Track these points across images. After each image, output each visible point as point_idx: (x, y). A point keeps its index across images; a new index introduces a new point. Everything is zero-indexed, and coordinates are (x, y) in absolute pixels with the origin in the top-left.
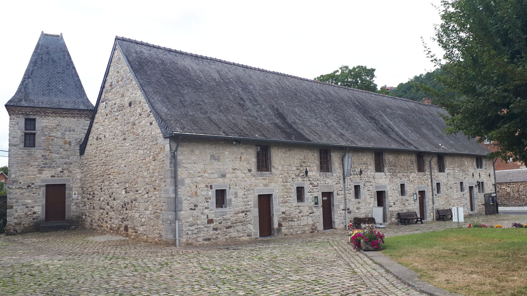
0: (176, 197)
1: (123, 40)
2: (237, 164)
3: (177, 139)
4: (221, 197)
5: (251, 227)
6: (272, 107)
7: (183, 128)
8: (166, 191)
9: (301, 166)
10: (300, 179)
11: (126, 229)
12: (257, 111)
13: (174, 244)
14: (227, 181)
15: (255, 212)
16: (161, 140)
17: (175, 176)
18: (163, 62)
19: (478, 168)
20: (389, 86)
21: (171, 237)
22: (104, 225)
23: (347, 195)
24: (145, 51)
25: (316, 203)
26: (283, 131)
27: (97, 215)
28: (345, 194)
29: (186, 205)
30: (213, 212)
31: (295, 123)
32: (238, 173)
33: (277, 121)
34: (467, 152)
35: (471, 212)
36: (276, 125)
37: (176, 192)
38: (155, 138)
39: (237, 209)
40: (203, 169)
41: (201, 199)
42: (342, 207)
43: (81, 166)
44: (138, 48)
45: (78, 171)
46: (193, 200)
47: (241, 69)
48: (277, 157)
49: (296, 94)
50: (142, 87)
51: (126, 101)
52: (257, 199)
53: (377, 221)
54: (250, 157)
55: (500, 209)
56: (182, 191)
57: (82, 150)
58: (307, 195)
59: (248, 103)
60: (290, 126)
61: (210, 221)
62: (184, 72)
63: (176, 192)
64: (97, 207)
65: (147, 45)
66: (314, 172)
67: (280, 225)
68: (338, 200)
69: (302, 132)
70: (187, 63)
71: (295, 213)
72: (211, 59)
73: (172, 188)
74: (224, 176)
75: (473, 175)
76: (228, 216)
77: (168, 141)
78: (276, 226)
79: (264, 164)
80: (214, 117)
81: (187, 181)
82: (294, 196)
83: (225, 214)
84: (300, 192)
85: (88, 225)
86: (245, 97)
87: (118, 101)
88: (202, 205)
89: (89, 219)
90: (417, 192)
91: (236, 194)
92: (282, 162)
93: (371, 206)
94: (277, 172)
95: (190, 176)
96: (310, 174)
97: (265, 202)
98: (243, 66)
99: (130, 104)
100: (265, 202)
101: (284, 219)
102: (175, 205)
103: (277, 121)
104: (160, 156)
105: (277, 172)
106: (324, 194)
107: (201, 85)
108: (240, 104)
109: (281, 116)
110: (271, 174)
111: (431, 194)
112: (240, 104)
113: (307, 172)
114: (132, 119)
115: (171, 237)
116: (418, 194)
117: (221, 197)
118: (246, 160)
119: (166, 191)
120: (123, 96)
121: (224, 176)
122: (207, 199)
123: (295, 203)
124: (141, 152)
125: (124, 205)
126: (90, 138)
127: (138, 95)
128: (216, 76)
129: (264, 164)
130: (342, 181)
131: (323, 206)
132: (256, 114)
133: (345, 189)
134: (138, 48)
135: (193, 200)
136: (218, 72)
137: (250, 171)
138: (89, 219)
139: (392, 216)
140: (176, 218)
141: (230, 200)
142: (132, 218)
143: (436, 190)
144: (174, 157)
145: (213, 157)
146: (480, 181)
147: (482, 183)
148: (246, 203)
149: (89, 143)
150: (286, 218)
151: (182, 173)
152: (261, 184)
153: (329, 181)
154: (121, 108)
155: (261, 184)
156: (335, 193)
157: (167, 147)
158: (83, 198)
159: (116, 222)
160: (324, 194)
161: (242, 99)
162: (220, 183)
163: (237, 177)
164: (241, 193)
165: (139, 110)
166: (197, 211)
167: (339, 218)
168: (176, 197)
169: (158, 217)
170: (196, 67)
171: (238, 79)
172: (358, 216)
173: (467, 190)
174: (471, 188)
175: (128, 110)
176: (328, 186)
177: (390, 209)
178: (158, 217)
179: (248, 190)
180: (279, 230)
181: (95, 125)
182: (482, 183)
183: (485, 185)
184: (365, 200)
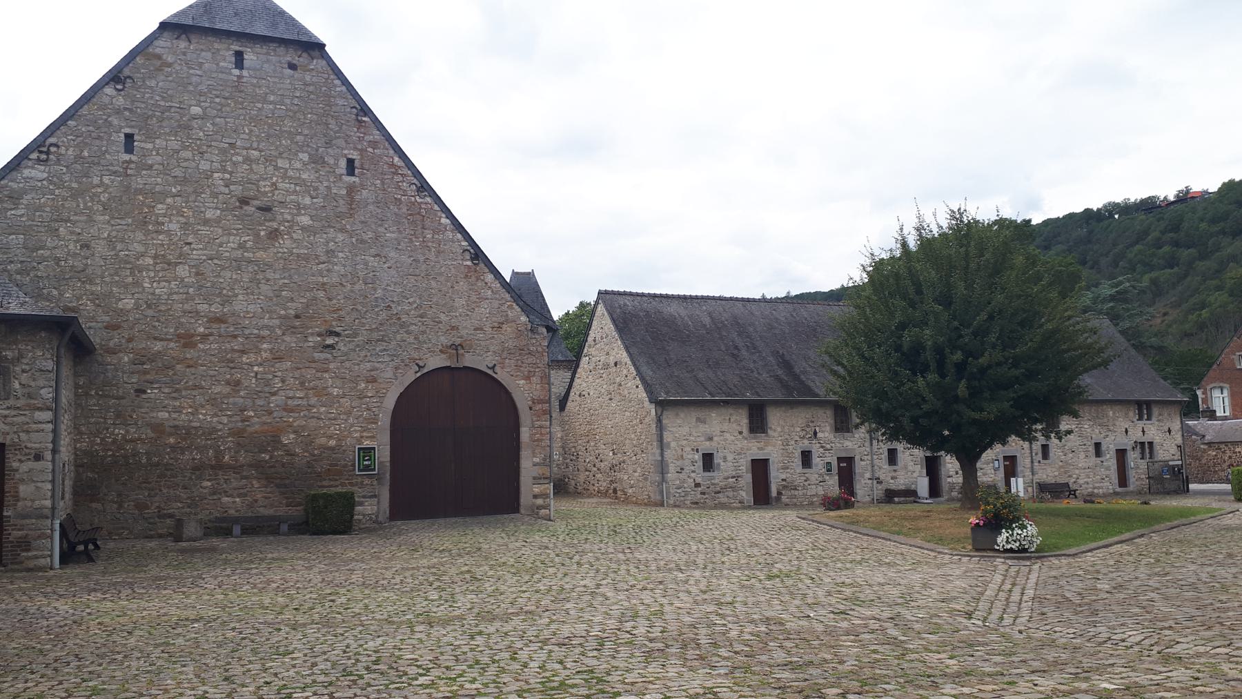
0: (662, 460)
1: (606, 292)
2: (726, 426)
3: (662, 405)
4: (708, 461)
5: (744, 494)
6: (775, 353)
7: (667, 393)
8: (654, 454)
9: (808, 426)
10: (806, 442)
11: (615, 491)
12: (754, 362)
13: (662, 505)
14: (714, 444)
15: (748, 477)
16: (647, 404)
17: (661, 439)
18: (648, 314)
19: (1140, 418)
20: (1196, 188)
21: (659, 498)
22: (591, 488)
23: (876, 462)
24: (628, 301)
25: (829, 470)
26: (784, 385)
27: (582, 478)
28: (872, 460)
29: (672, 468)
30: (700, 476)
31: (805, 372)
32: (727, 435)
33: (780, 372)
34: (1110, 396)
35: (1119, 490)
36: (777, 378)
37: (662, 455)
38: (641, 402)
39: (726, 474)
40: (687, 433)
41: (687, 462)
42: (868, 475)
43: (562, 424)
44: (621, 300)
45: (558, 428)
46: (679, 463)
47: (739, 305)
48: (776, 419)
49: (815, 330)
50: (627, 349)
51: (612, 360)
52: (749, 464)
53: (920, 494)
54: (741, 419)
55: (1192, 486)
56: (668, 454)
57: (562, 407)
58: (816, 460)
59: (744, 352)
60: (796, 377)
61: (698, 485)
62: (670, 322)
63: (662, 455)
64: (582, 469)
65: (631, 294)
66: (826, 433)
67: (779, 493)
68: (861, 467)
69: (812, 384)
70: (673, 309)
71: (799, 481)
72: (703, 298)
73: (658, 452)
74: (711, 439)
75: (1126, 431)
76: (716, 481)
77: (653, 406)
78: (774, 493)
79: (758, 425)
80: (701, 375)
81: (673, 444)
82: (798, 461)
83: (713, 478)
84: (806, 458)
85: (571, 489)
86: (741, 345)
87: (603, 359)
88: (688, 468)
89: (573, 483)
90: (1001, 457)
91: (725, 458)
92: (781, 422)
93: (915, 475)
94: (776, 434)
95: (676, 439)
96: (820, 435)
97: (760, 468)
98: (743, 300)
99: (616, 364)
100: (760, 468)
101: (785, 487)
102: (662, 467)
103: (780, 372)
104: (647, 420)
105: (776, 434)
106: (840, 460)
107: (688, 336)
108: (733, 355)
109: (787, 365)
110: (767, 436)
111: (1028, 461)
112: (733, 355)
113: (815, 433)
114: (618, 380)
115: (659, 498)
116: (1002, 460)
117: (708, 461)
118: (736, 421)
119: (654, 454)
120: (608, 354)
121: (711, 439)
122: (693, 463)
123: (799, 469)
124: (627, 414)
125: (612, 467)
126: (572, 394)
127: (624, 356)
128: (707, 320)
129: (758, 425)
130: (867, 444)
131: (840, 474)
132: (752, 366)
133: (872, 453)
134: (621, 300)
135: (679, 463)
136: (710, 314)
137: (741, 433)
138: (573, 483)
139: (951, 489)
140: (663, 480)
141: (719, 464)
142: (621, 480)
143: (1040, 455)
144: (659, 421)
145: (698, 420)
146: (1146, 439)
147: (1151, 444)
148: (737, 468)
149: (570, 399)
150: (787, 486)
151: (667, 437)
152: (755, 448)
153: (848, 444)
154: (606, 366)
155: (755, 448)
156: (857, 458)
157: (653, 411)
158: (565, 459)
159: (604, 485)
160: (840, 460)
161: (736, 348)
162: (706, 447)
163: (726, 440)
164: (730, 457)
165: (625, 372)
166: (684, 468)
167: (862, 487)
168: (662, 460)
169: (646, 479)
170: (683, 313)
171: (736, 321)
172: (893, 487)
173: (1110, 460)
174: (1121, 454)
175: (614, 369)
176: (846, 450)
177: (949, 480)
178: (646, 479)
179: (739, 454)
180: (778, 498)
181: (577, 381)
182: (1151, 444)
183: (1157, 448)
184: (906, 467)
